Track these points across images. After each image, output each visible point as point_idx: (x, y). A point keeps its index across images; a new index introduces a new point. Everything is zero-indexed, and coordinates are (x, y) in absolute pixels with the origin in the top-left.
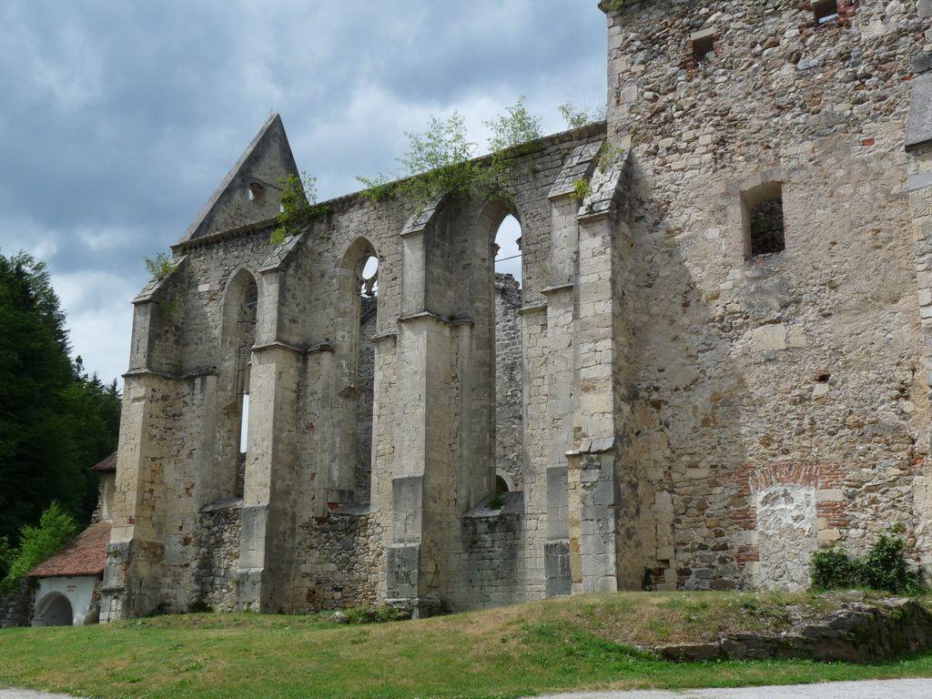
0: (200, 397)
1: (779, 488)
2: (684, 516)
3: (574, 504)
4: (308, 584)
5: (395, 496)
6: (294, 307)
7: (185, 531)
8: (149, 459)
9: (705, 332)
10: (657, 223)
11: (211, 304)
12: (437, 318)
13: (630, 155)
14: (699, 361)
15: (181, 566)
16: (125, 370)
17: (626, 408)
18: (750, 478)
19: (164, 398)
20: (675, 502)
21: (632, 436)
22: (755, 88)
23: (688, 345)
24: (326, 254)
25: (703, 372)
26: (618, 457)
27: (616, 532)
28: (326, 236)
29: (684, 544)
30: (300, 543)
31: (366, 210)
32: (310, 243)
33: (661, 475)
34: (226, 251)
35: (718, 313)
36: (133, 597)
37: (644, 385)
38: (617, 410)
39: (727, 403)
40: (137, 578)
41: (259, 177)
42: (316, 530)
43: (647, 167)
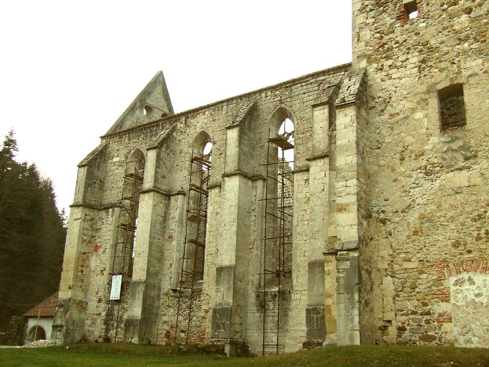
0: (111, 219)
1: (465, 276)
2: (402, 292)
3: (330, 283)
4: (166, 327)
5: (217, 278)
6: (164, 169)
7: (99, 295)
8: (82, 253)
9: (415, 176)
10: (382, 111)
11: (120, 168)
12: (244, 176)
13: (366, 70)
14: (411, 194)
15: (97, 315)
16: (72, 203)
17: (365, 223)
18: (446, 269)
19: (92, 219)
20: (395, 284)
21: (368, 241)
22: (444, 29)
23: (404, 184)
24: (183, 141)
25: (414, 201)
26: (361, 254)
27: (360, 302)
28: (184, 130)
29: (402, 311)
30: (163, 304)
31: (206, 116)
32: (174, 134)
33: (386, 266)
34: (129, 139)
35: (423, 164)
36: (69, 331)
37: (375, 209)
38: (360, 224)
39: (430, 220)
40: (72, 320)
41: (150, 103)
42: (172, 296)
43: (376, 77)
